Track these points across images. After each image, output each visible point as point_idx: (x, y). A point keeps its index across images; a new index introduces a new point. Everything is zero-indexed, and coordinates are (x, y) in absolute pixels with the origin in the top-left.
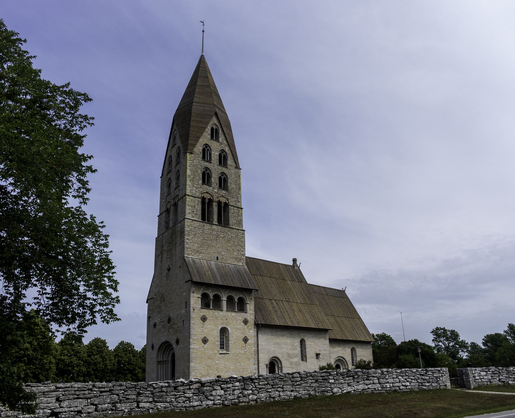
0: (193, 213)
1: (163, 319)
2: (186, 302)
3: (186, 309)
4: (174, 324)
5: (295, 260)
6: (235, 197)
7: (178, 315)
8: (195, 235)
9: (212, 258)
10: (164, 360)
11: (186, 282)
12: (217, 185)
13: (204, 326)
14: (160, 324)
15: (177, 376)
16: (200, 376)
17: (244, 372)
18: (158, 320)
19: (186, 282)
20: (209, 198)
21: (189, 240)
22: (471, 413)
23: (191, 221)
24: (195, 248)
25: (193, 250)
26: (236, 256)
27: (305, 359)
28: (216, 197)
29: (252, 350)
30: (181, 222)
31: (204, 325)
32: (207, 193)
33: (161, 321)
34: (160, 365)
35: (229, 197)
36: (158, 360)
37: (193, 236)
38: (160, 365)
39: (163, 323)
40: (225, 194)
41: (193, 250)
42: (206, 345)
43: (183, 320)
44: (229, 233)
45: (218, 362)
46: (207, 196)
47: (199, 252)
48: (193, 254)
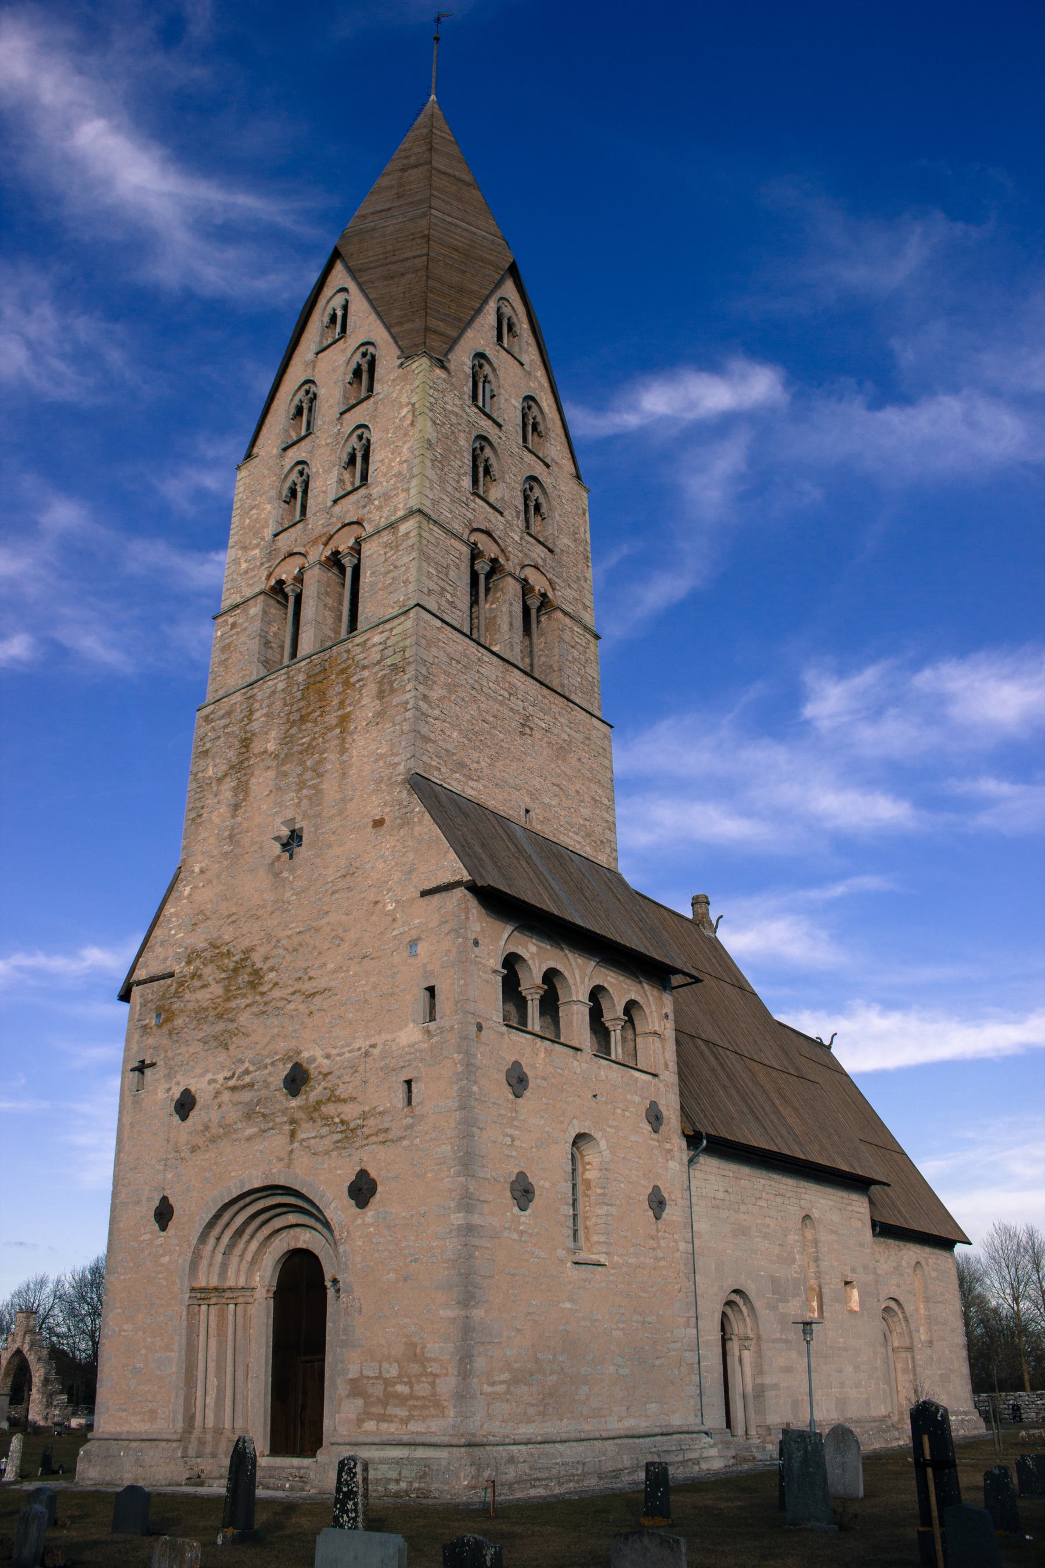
0: (442, 595)
1: (247, 1072)
2: (431, 990)
3: (432, 1026)
4: (334, 1098)
5: (699, 902)
6: (575, 586)
7: (367, 1054)
8: (452, 688)
9: (512, 808)
10: (230, 1283)
11: (425, 894)
12: (518, 517)
13: (514, 1119)
14: (226, 1096)
15: (353, 1372)
16: (506, 1376)
17: (658, 1362)
18: (213, 1081)
19: (425, 894)
20: (493, 556)
21: (432, 708)
22: (193, 1401)
23: (438, 623)
24: (450, 747)
25: (443, 753)
26: (587, 823)
27: (815, 1304)
28: (516, 561)
29: (677, 1255)
30: (388, 626)
31: (516, 1111)
32: (488, 533)
33: (232, 1083)
34: (204, 1308)
35: (557, 580)
36: (196, 1285)
37: (444, 693)
38: (204, 1308)
39: (247, 1096)
40: (544, 560)
41: (443, 753)
42: (525, 1216)
43: (409, 1082)
44: (563, 720)
45: (568, 1305)
46: (490, 549)
47: (466, 771)
48: (444, 770)
